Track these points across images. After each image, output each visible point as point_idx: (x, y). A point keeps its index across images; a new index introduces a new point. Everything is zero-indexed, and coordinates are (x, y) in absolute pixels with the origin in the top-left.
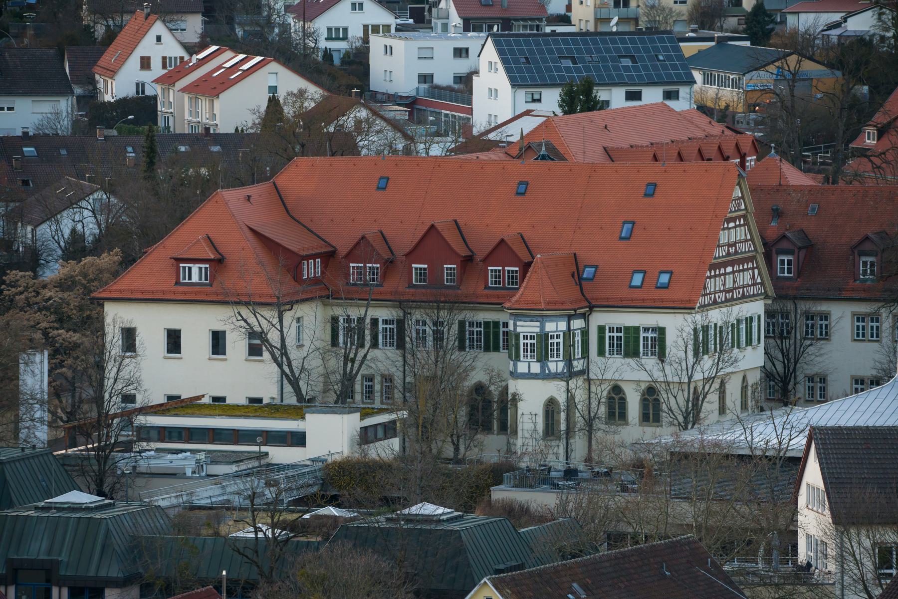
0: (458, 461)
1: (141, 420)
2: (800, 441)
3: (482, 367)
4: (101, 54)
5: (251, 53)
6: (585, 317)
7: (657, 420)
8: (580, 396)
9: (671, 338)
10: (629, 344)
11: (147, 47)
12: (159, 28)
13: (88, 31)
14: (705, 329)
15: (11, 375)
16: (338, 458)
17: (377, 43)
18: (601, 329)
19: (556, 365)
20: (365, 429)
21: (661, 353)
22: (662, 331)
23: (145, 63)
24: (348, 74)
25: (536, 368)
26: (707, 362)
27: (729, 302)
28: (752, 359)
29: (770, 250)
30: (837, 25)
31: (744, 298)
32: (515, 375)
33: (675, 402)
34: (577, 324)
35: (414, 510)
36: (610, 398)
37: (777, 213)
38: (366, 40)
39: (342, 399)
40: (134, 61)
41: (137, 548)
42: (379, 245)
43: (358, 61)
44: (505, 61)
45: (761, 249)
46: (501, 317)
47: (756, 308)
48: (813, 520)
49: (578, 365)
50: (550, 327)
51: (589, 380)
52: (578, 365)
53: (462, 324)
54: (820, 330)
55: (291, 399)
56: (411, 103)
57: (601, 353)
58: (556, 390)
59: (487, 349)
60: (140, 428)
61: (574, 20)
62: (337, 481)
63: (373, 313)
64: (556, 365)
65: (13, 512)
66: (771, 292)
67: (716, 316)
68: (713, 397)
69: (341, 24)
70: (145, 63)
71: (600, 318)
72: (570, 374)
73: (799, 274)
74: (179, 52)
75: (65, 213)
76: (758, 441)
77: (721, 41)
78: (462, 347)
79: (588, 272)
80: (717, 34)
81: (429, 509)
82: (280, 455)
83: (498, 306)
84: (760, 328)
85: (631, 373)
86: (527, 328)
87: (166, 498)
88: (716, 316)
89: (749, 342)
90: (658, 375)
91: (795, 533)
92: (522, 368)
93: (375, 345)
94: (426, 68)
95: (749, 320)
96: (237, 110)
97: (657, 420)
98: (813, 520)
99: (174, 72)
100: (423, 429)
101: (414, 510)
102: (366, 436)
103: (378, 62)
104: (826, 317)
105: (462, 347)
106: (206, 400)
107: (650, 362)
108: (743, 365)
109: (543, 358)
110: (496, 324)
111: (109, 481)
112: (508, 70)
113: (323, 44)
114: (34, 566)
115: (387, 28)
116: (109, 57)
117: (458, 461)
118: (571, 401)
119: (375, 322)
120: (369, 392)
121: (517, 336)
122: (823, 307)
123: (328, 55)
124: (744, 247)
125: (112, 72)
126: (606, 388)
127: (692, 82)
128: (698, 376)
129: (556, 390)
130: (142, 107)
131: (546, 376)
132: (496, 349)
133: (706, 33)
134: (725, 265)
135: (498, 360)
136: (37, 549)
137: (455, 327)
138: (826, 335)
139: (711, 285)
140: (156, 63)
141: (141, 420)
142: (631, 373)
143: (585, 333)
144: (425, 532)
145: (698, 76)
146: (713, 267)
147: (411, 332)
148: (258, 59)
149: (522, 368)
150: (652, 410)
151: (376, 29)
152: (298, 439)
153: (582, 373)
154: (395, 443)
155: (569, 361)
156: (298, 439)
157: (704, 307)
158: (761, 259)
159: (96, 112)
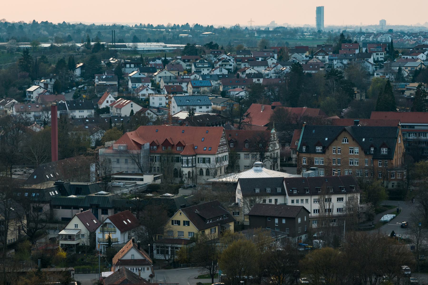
0: (172, 183)
1: (112, 176)
2: (237, 180)
3: (177, 165)
4: (99, 100)
5: (128, 99)
6: (195, 156)
7: (209, 175)
8: (195, 170)
9: (211, 160)
10: (204, 161)
11: (108, 99)
12: (110, 95)
13: (96, 96)
14: (218, 158)
15: (89, 168)
16: (150, 183)
17: (151, 98)
18: (198, 158)
19: (190, 165)
20: (154, 178)
21: (210, 163)
22: (210, 158)
23: (107, 102)
24: (145, 103)
25: (186, 166)
26: (218, 164)
27: (222, 153)
28: (226, 163)
29: (229, 142)
30: (238, 94)
31: (225, 152)
32: (183, 167)
33: (212, 172)
34: (194, 157)
35: (166, 195)
36: (200, 171)
37: (230, 135)
38: (149, 96)
39: (150, 172)
40: (105, 101)
41: (114, 201)
42: (156, 142)
43: (148, 100)
44: (176, 101)
45: (228, 143)
46: (180, 156)
47: (227, 154)
48: (239, 196)
49: (194, 165)
50: (189, 158)
51: (196, 168)
52: (194, 165)
53: (172, 157)
54: (238, 157)
55: (140, 172)
56: (158, 108)
57: (198, 162)
58: (190, 170)
59: (177, 162)
60: (113, 178)
61: (188, 92)
62: (151, 188)
63: (155, 155)
64: (190, 165)
65: (91, 195)
66: (230, 150)
67: (220, 155)
68: (219, 171)
69: (144, 93)
70: (107, 102)
71: (198, 156)
72: (192, 167)
73: (234, 147)
74: (114, 99)
75: (95, 133)
76: (228, 180)
77: (216, 97)
78: (172, 162)
79: (196, 148)
80: (216, 95)
81: (169, 195)
82: (139, 183)
83: (179, 154)
84: (228, 158)
85: (204, 166)
86: (185, 158)
87: (118, 192)
88: (220, 155)
89: (226, 160)
90: (209, 167)
91: (235, 197)
92: (184, 166)
93: (156, 161)
94: (161, 102)
95: (226, 156)
96: (126, 112)
97: (209, 175)
98: (239, 196)
99: (113, 103)
100: (164, 177)
101: (166, 195)
102: (155, 179)
103: (151, 100)
104: (239, 155)
105: (172, 162)
106: (124, 172)
107: (208, 164)
108: (224, 165)
109: (188, 164)
110: (179, 157)
111: (107, 188)
112: (176, 103)
113: (141, 97)
114: (95, 205)
115: (153, 94)
116: (101, 101)
117: (172, 183)
118: (193, 171)
119: (156, 157)
120: (155, 170)
121: (183, 160)
122: (239, 153)
123: (142, 99)
124: (225, 142)
125: (101, 104)
126: (199, 169)
127: (211, 105)
128: (216, 167)
129: (190, 170)
130: (107, 110)
131: (188, 167)
132: (179, 162)
133: (213, 95)
134: (221, 146)
135: (179, 164)
136: (95, 202)
137: (171, 158)
138: (239, 158)
139: (219, 150)
140: (109, 102)
141: (112, 176)
142: (204, 166)
143: (195, 159)
144: (168, 200)
145: (212, 104)
146: (219, 146)
147: (162, 159)
148: (129, 101)
149: (184, 166)
150: (208, 173)
151: (151, 94)
152: (142, 180)
153: (195, 166)
154: (160, 180)
155: (192, 164)
156: (142, 180)
157: (217, 154)
158: (228, 144)
159: (99, 112)
